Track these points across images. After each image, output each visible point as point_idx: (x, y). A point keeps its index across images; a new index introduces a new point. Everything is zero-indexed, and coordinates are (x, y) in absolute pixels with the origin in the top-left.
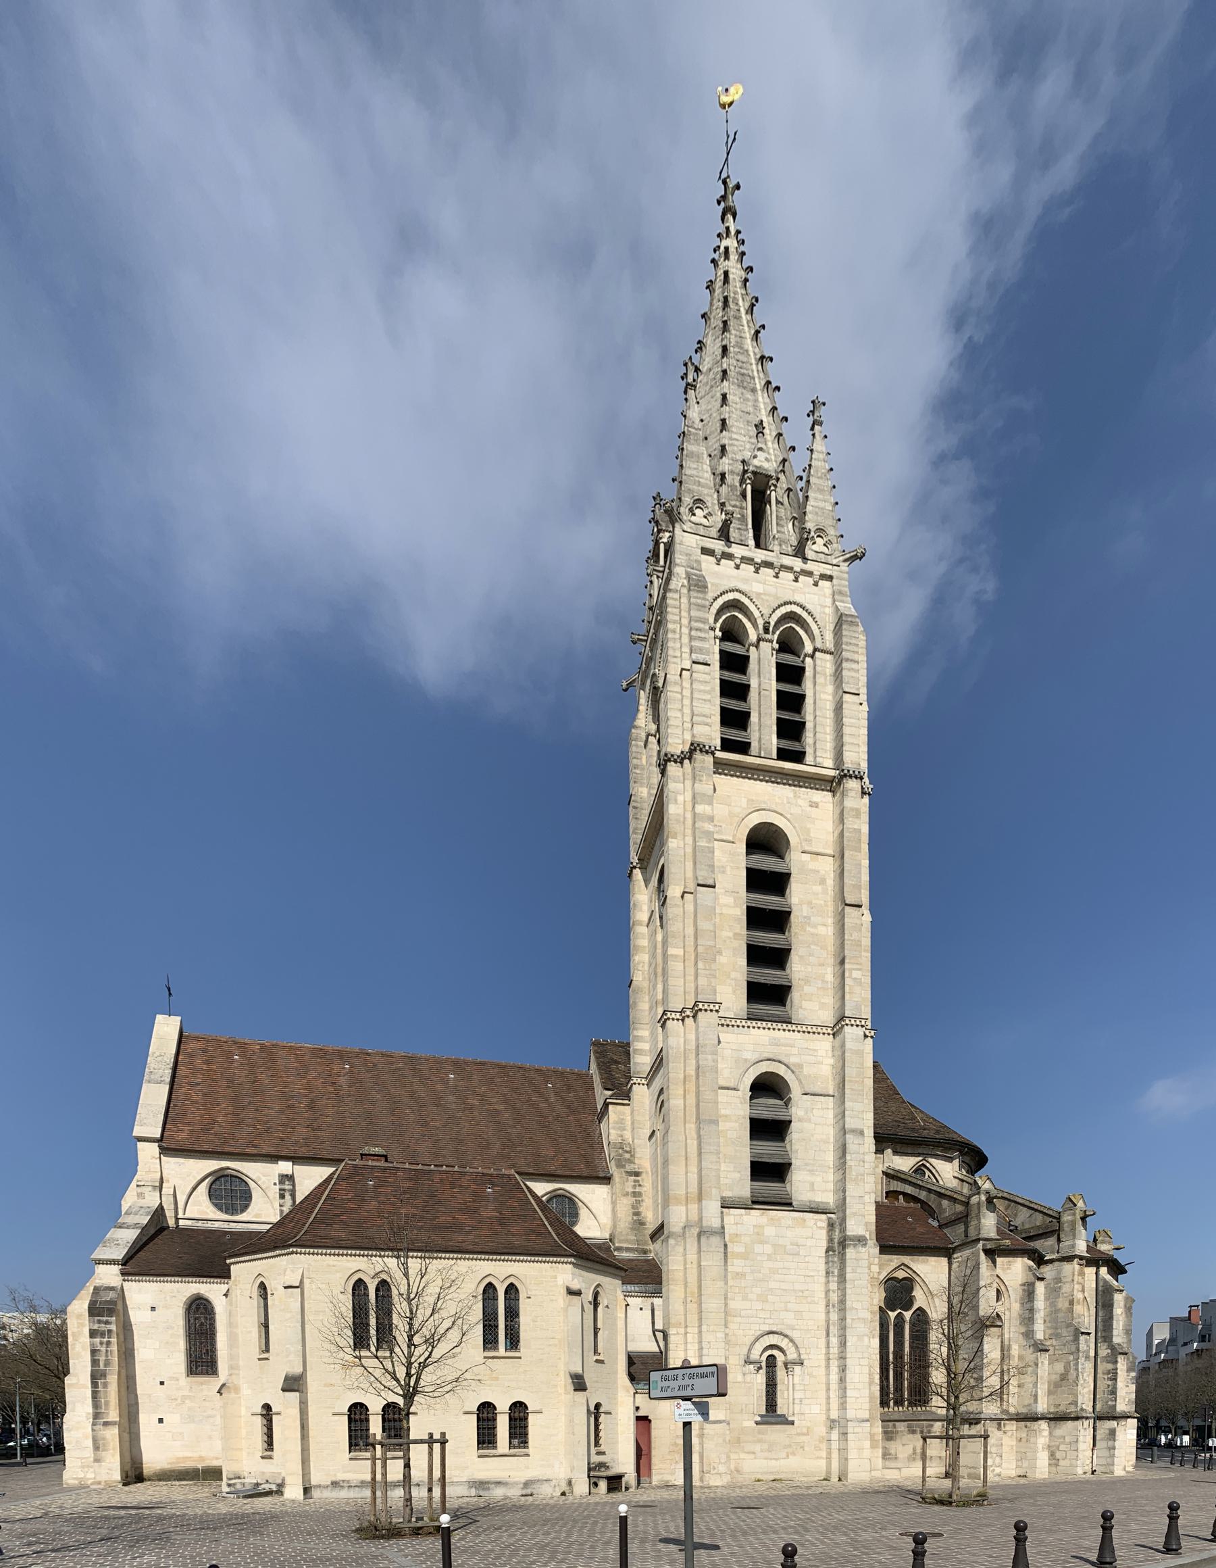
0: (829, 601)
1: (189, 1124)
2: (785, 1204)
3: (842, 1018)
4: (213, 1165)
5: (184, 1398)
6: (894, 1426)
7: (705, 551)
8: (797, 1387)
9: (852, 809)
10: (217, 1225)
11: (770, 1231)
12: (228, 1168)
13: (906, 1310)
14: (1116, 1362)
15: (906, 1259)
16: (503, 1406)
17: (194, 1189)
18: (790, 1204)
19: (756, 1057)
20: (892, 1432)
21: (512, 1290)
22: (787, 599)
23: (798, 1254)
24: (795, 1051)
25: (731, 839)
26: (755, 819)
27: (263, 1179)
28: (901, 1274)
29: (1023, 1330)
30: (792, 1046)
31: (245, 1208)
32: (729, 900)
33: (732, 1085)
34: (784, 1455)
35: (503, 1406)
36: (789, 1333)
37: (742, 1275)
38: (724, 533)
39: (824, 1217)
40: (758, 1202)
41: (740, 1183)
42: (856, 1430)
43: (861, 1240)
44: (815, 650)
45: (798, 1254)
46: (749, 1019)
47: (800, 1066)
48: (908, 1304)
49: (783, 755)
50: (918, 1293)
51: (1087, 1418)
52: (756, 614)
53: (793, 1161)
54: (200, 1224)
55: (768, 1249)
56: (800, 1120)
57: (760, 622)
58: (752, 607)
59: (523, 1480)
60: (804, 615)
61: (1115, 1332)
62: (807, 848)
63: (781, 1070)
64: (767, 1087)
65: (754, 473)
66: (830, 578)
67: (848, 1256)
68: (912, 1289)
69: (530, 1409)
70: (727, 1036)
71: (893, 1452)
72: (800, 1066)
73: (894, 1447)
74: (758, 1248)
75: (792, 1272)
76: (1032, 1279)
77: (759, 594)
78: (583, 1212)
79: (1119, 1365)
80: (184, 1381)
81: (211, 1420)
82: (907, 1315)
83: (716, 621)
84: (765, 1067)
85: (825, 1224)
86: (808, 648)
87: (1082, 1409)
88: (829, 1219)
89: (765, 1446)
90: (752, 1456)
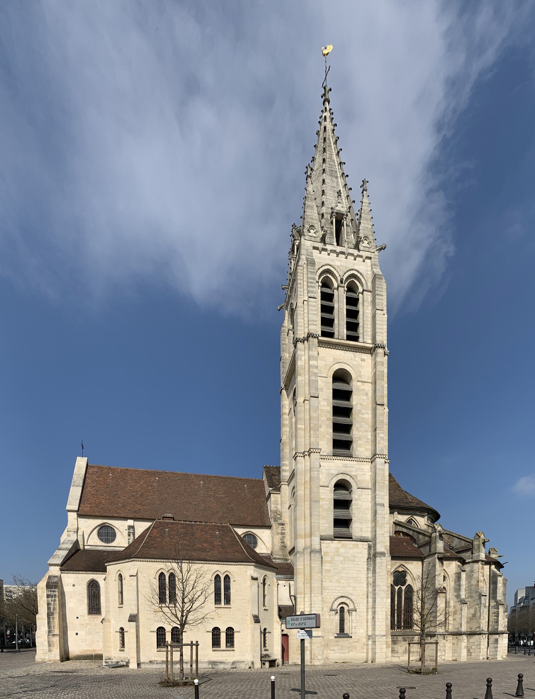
0: (370, 268)
1: (90, 504)
2: (349, 538)
3: (375, 455)
4: (100, 522)
5: (87, 624)
6: (397, 638)
7: (315, 248)
8: (353, 621)
9: (380, 362)
10: (101, 548)
11: (342, 550)
12: (106, 523)
13: (403, 586)
14: (498, 608)
15: (403, 562)
16: (223, 629)
17: (92, 532)
18: (351, 538)
19: (336, 472)
20: (396, 641)
21: (227, 578)
22: (351, 268)
23: (354, 561)
24: (354, 469)
25: (326, 376)
26: (337, 367)
27: (121, 527)
28: (401, 569)
29: (456, 594)
30: (353, 467)
31: (113, 541)
32: (325, 403)
33: (326, 485)
34: (347, 651)
35: (223, 629)
36: (350, 597)
37: (329, 571)
38: (323, 240)
39: (366, 543)
40: (337, 537)
41: (329, 528)
42: (380, 640)
43: (383, 554)
44: (363, 290)
45: (354, 561)
46: (333, 456)
47: (356, 476)
48: (404, 583)
49: (349, 338)
50: (408, 578)
51: (485, 634)
52: (337, 275)
53: (353, 518)
54: (94, 548)
55: (341, 559)
56: (356, 500)
57: (339, 279)
58: (335, 272)
59: (232, 662)
60: (359, 275)
61: (498, 595)
62: (360, 380)
63: (348, 478)
64: (342, 485)
65: (337, 213)
66: (370, 258)
67: (377, 561)
68: (406, 576)
69: (221, 631)
70: (324, 463)
71: (396, 649)
72: (356, 476)
73: (397, 647)
74: (337, 558)
75: (352, 569)
76: (460, 571)
77: (338, 266)
78: (259, 542)
79: (500, 610)
80: (87, 617)
81: (98, 634)
82: (403, 588)
83: (319, 278)
84: (340, 477)
85: (367, 547)
86: (360, 290)
87: (482, 630)
88: (369, 544)
89: (340, 647)
90: (334, 652)
